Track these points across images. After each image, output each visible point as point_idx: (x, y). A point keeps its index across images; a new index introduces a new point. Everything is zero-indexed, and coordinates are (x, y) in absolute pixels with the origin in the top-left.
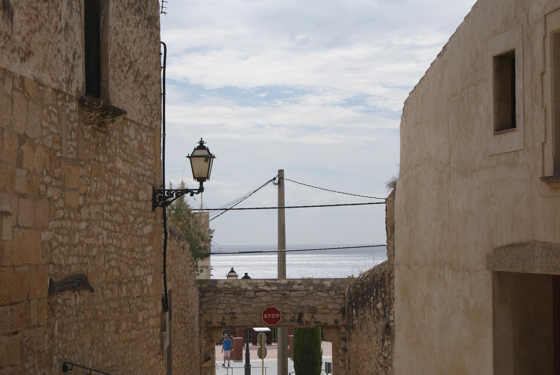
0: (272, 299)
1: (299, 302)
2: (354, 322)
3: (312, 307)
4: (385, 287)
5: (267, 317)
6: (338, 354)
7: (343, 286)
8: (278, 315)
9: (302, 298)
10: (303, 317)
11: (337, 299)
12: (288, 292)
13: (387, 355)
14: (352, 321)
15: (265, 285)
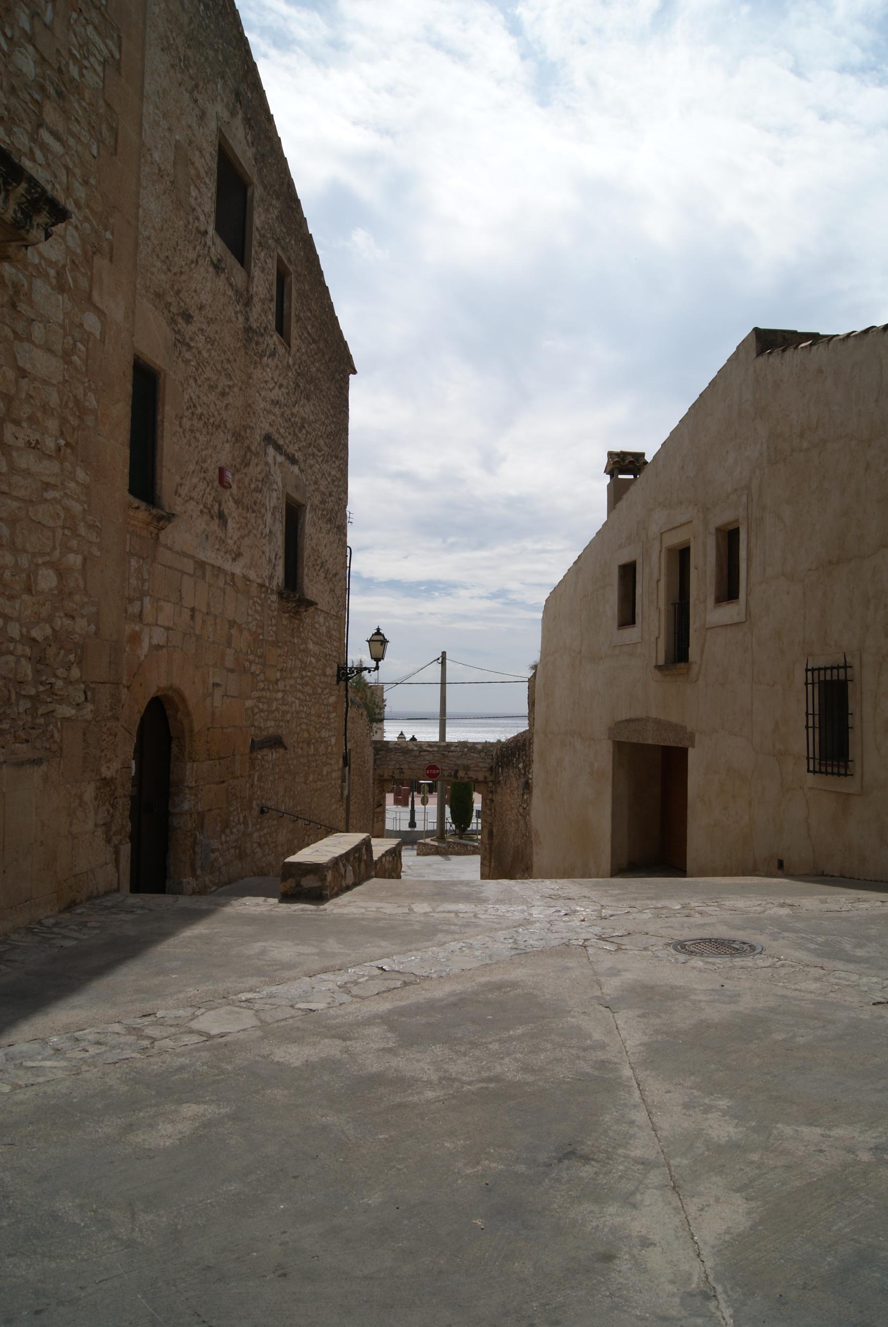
4: (525, 750)
8: (438, 771)
12: (446, 753)
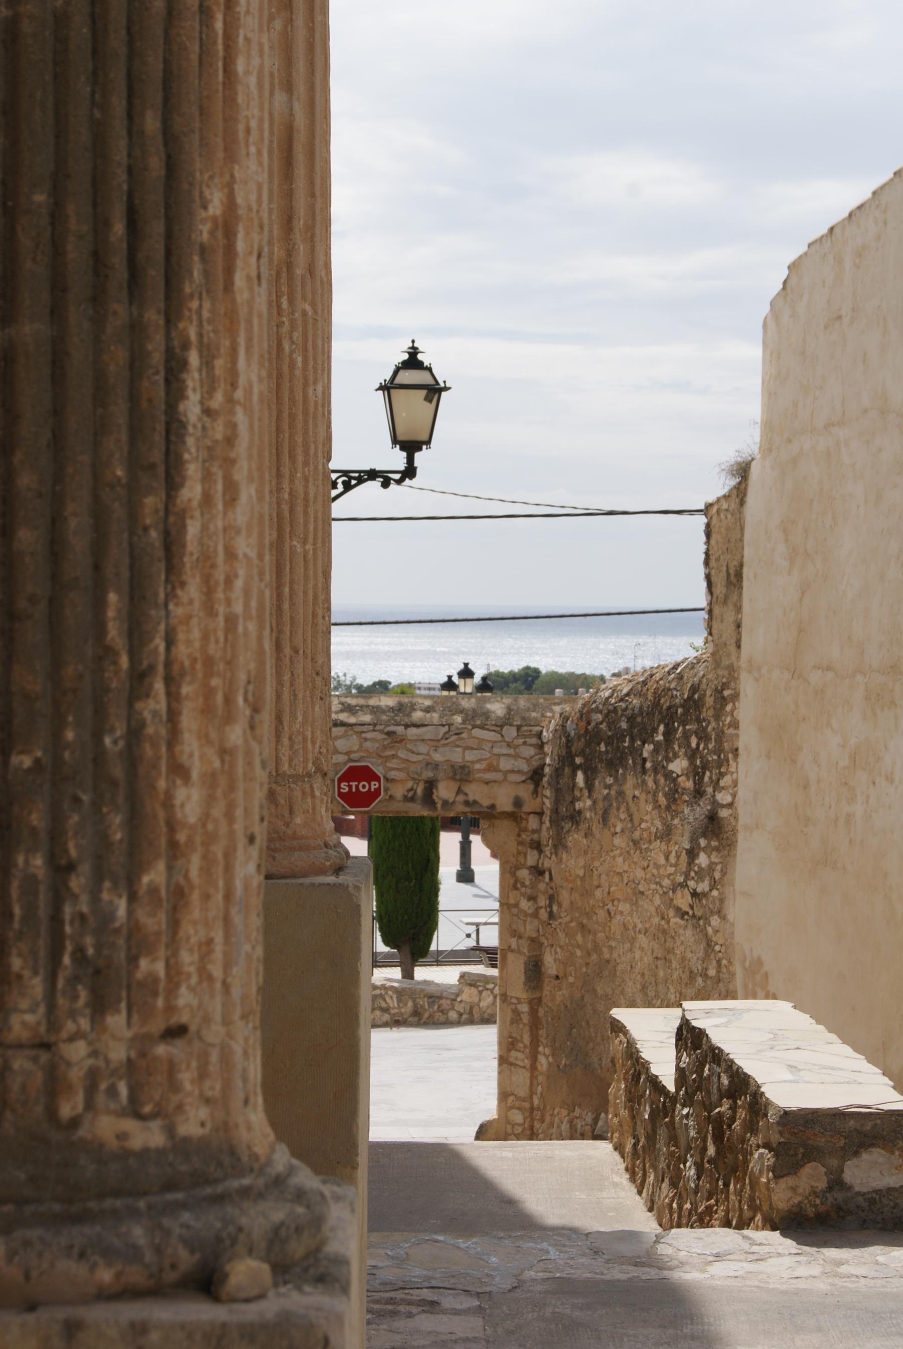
0: (361, 746)
1: (428, 754)
2: (578, 805)
3: (460, 767)
4: (699, 721)
5: (347, 789)
6: (516, 882)
7: (534, 714)
8: (374, 785)
9: (435, 744)
10: (437, 791)
11: (521, 747)
12: (400, 729)
13: (707, 889)
14: (572, 802)
15: (342, 711)
